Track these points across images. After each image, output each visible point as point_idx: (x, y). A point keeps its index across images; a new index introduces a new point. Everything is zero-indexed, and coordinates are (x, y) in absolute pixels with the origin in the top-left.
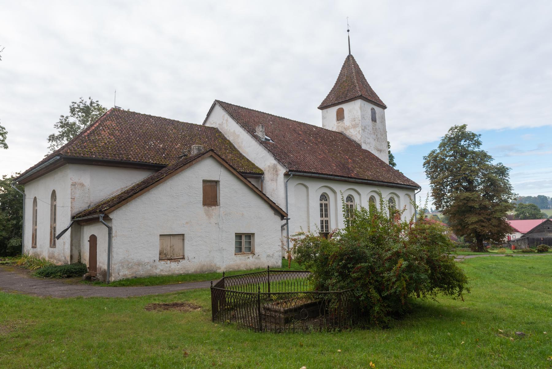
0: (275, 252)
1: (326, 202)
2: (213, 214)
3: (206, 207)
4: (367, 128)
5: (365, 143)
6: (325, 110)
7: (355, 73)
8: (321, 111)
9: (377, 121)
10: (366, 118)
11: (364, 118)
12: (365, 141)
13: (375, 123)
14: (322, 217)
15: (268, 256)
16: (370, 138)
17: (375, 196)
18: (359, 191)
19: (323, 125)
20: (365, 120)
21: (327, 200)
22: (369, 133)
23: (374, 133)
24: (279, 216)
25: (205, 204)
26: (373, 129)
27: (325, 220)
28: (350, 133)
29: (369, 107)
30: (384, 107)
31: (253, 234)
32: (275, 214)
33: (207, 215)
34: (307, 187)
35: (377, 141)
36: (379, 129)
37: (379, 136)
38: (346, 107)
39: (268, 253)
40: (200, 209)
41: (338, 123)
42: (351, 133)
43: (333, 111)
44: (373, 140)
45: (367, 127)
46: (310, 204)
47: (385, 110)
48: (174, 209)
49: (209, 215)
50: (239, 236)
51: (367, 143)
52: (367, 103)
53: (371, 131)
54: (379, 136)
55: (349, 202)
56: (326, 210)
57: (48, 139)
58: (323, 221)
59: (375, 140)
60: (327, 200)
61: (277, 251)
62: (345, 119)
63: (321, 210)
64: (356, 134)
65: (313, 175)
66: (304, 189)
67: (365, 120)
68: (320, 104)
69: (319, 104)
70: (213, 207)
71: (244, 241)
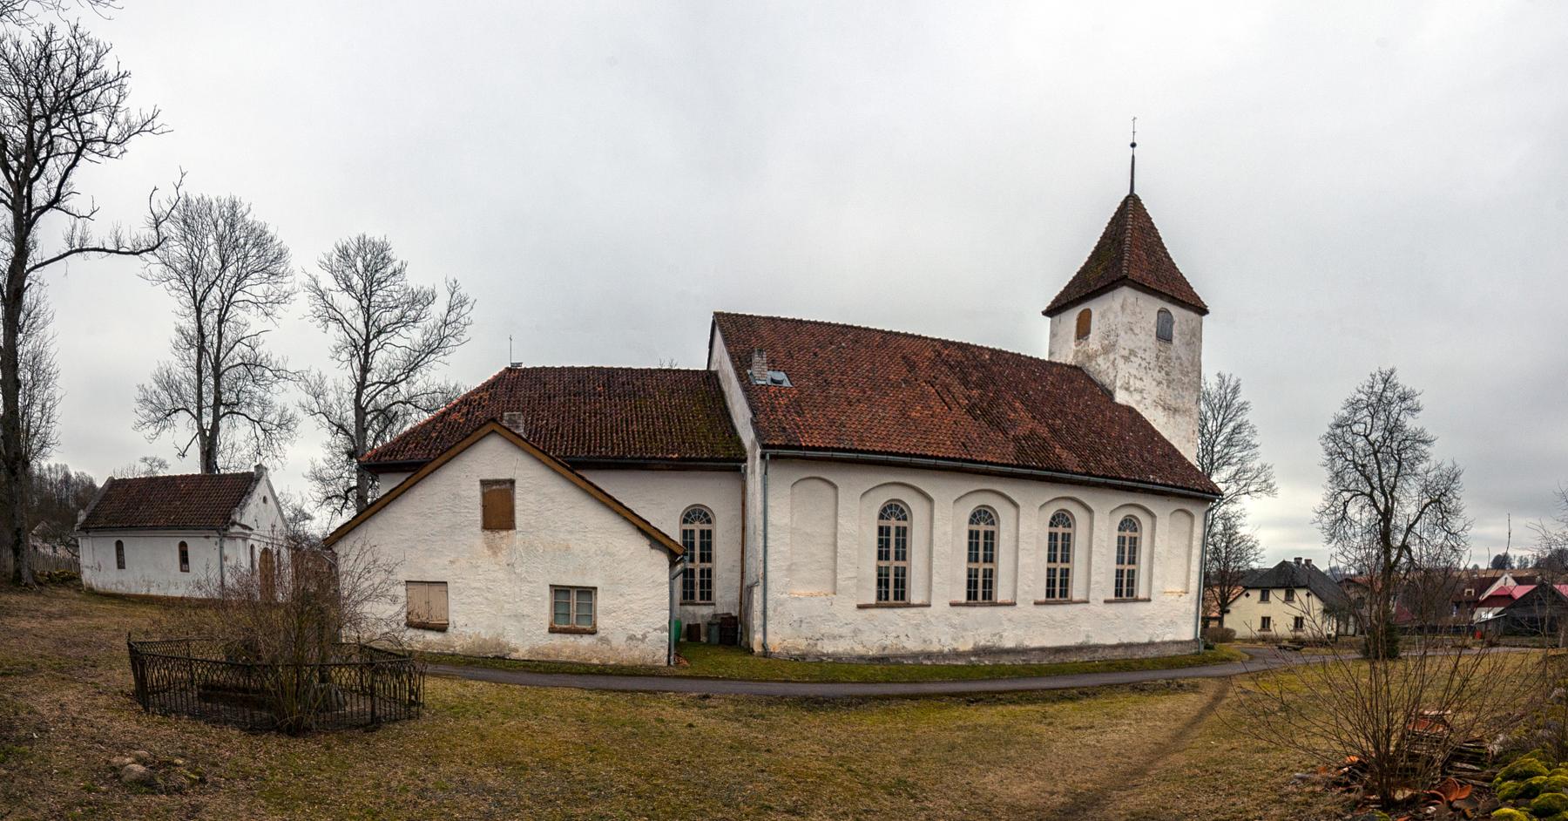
0: (651, 630)
1: (1134, 534)
2: (504, 546)
3: (486, 532)
4: (1139, 356)
5: (1127, 389)
6: (1057, 318)
7: (1130, 231)
8: (1049, 319)
9: (1175, 341)
10: (1137, 331)
11: (1131, 330)
12: (1128, 383)
13: (1168, 345)
14: (1123, 563)
15: (632, 638)
16: (1144, 378)
17: (1135, 515)
18: (922, 488)
19: (1051, 354)
20: (1136, 335)
21: (1069, 526)
22: (1143, 366)
23: (1161, 367)
24: (664, 552)
25: (487, 526)
26: (1158, 357)
27: (1129, 571)
28: (1097, 367)
29: (1149, 308)
30: (1202, 310)
31: (595, 588)
32: (652, 547)
33: (490, 547)
34: (835, 487)
35: (1168, 387)
36: (1179, 358)
37: (1176, 375)
38: (1096, 307)
39: (631, 632)
40: (475, 536)
41: (1076, 346)
42: (1099, 365)
43: (1071, 318)
44: (1154, 383)
45: (1140, 353)
46: (839, 527)
47: (1204, 318)
48: (426, 537)
49: (494, 549)
50: (559, 591)
51: (1132, 389)
52: (1147, 297)
53: (1149, 363)
54: (1176, 375)
55: (982, 524)
56: (1133, 550)
57: (142, 388)
58: (1055, 570)
59: (1159, 383)
60: (1136, 530)
61: (655, 630)
62: (1091, 335)
63: (1121, 550)
64: (1108, 368)
65: (940, 462)
66: (829, 491)
67: (1136, 335)
68: (1049, 304)
69: (1046, 303)
70: (504, 533)
71: (575, 602)
